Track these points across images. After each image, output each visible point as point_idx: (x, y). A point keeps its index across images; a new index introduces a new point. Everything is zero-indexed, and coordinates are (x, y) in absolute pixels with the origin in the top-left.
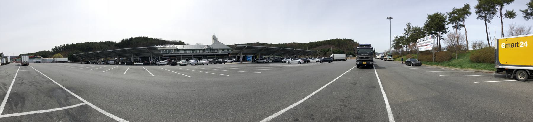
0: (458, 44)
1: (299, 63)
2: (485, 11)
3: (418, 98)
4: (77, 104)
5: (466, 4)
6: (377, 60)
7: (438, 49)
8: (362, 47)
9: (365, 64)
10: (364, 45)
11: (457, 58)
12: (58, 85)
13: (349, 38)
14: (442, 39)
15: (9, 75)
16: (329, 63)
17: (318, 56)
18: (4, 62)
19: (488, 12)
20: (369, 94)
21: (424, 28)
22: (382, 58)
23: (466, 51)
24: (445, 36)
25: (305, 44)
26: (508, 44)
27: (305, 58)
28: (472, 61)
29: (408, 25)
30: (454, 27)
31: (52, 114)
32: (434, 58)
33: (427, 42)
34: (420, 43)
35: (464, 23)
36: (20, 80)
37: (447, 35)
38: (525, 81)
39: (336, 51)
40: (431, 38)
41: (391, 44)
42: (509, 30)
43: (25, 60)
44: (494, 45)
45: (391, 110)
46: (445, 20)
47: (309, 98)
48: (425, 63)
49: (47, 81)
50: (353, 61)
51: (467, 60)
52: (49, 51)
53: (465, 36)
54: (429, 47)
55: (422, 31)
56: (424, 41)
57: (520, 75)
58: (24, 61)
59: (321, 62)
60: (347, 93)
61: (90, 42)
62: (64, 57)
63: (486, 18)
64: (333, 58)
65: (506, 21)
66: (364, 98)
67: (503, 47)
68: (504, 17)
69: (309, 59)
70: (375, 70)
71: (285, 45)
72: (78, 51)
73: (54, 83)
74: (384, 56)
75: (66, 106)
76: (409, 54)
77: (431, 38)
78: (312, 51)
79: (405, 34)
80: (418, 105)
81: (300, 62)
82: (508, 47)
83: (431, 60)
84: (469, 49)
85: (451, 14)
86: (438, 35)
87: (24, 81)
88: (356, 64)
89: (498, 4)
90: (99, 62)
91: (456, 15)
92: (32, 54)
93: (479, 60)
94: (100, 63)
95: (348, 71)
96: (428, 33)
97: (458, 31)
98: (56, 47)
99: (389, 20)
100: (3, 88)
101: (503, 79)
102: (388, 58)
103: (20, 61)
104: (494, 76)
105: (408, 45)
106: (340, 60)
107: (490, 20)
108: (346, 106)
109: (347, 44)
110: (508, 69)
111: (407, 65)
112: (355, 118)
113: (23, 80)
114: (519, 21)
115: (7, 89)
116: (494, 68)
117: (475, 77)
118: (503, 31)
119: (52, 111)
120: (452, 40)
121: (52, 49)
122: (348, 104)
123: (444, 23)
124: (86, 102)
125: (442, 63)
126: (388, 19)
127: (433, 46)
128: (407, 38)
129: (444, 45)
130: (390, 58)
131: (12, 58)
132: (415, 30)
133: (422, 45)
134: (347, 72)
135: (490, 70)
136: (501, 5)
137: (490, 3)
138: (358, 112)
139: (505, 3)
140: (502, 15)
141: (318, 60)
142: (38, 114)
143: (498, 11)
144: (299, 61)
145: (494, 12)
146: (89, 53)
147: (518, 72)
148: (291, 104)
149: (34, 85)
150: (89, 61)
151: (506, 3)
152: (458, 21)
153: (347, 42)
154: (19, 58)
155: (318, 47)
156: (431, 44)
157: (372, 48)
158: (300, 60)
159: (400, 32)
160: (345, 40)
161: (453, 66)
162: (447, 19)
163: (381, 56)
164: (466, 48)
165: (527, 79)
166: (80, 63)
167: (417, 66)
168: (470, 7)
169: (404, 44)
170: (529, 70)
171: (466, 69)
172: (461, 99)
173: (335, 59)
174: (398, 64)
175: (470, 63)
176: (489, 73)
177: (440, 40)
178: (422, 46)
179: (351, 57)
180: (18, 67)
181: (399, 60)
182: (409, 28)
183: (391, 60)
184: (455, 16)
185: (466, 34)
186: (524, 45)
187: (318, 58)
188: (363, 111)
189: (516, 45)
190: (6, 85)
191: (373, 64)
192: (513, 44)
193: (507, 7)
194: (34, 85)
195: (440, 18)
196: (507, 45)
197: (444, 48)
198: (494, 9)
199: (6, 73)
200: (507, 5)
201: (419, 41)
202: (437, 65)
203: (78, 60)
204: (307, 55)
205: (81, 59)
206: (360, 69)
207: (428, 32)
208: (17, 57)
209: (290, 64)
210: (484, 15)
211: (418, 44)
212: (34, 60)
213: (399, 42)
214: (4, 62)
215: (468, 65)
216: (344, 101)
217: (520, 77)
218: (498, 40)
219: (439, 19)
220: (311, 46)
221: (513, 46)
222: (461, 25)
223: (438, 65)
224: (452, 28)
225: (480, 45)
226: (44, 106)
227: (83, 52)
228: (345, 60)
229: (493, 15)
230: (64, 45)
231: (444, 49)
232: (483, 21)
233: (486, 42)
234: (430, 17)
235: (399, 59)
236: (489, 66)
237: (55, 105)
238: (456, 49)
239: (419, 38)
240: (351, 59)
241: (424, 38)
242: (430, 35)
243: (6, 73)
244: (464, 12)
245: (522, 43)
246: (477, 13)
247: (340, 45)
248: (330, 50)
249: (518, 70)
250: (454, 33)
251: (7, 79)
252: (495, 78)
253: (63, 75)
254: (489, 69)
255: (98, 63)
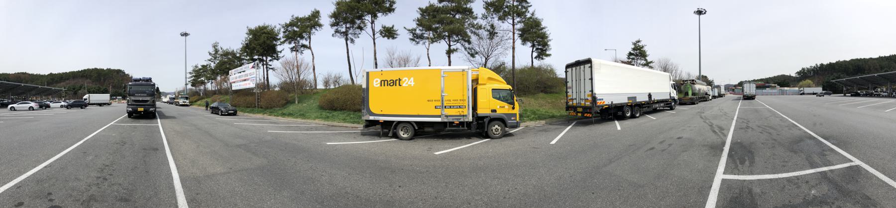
0: (299, 79)
1: (31, 108)
2: (345, 23)
3: (231, 169)
4: (841, 164)
5: (315, 9)
6: (161, 105)
7: (265, 86)
8: (137, 82)
9: (141, 112)
10: (140, 80)
11: (297, 102)
12: (808, 133)
13: (116, 68)
14: (272, 69)
15: (725, 114)
16: (82, 108)
17: (63, 97)
18: (716, 94)
19: (351, 25)
20: (145, 161)
21: (240, 51)
22: (172, 101)
23: (312, 90)
24: (275, 64)
25: (42, 76)
26: (384, 81)
27: (41, 100)
28: (322, 108)
29: (215, 46)
30: (292, 49)
31: (798, 179)
32: (258, 102)
33: (246, 75)
34: (234, 76)
35: (310, 42)
36: (743, 122)
37: (281, 63)
38: (411, 139)
39: (93, 89)
40: (253, 67)
41: (186, 78)
42: (386, 57)
43: (750, 90)
44: (360, 81)
45: (183, 188)
46: (278, 36)
47: (45, 167)
48: (243, 110)
49: (787, 126)
50: (121, 106)
51: (314, 105)
52: (792, 75)
53: (311, 64)
54: (250, 84)
55: (238, 55)
56: (240, 72)
57: (403, 130)
58: (748, 92)
59: (69, 107)
60: (109, 157)
61: (861, 59)
62: (817, 85)
63: (347, 35)
64: (88, 100)
65: (382, 41)
66: (136, 167)
67: (377, 84)
68: (378, 35)
69: (48, 103)
70: (159, 120)
71: (6, 77)
72: (839, 74)
73: (800, 129)
74: (174, 99)
75: (821, 167)
76: (217, 95)
77: (253, 67)
78: (53, 88)
79: (209, 60)
80: (231, 180)
81: (32, 107)
82: (384, 86)
83: (253, 105)
84: (318, 88)
85: (288, 27)
86: (265, 63)
87: (750, 125)
88: (127, 110)
89: (369, 13)
90: (877, 93)
91: (295, 29)
92: (761, 80)
93: (334, 106)
94: (879, 95)
95: (112, 123)
96: (248, 60)
97: (299, 55)
98: (803, 69)
99: (184, 37)
100: (719, 134)
101: (376, 137)
102: (181, 101)
103: (741, 91)
104: (360, 134)
105: (215, 79)
106: (100, 105)
107: (354, 38)
108: (106, 180)
109: (113, 78)
110: (384, 121)
111: (212, 113)
112: (119, 200)
113: (749, 123)
114: (403, 44)
115: (726, 136)
116: (360, 121)
117: (328, 134)
118: (376, 59)
119: (798, 175)
120: (289, 71)
121: (796, 73)
122: (109, 176)
123: (275, 42)
124: (857, 162)
125: (271, 110)
126: (182, 35)
127: (256, 80)
128: (213, 67)
129: (275, 80)
130: (185, 101)
131: (728, 88)
132: (226, 54)
133: (238, 79)
134: (110, 124)
135: (354, 122)
136: (374, 16)
137: (356, 11)
138: (125, 189)
139: (379, 12)
140: (375, 33)
141: (63, 103)
142: (776, 179)
143: (369, 25)
144: (30, 105)
145: (362, 25)
146: (858, 77)
147: (401, 126)
148: (11, 180)
149: (767, 132)
150: (859, 92)
151: (382, 12)
152: (298, 39)
153: (112, 74)
154: (739, 88)
155: (63, 82)
156: (253, 79)
157: (154, 85)
158: (33, 104)
159: (202, 58)
160: (109, 70)
161: (290, 115)
162: (281, 35)
163: (170, 98)
164: (313, 84)
165: (414, 136)
166: (843, 95)
167: (229, 115)
168: (321, 16)
169: (209, 79)
170: (416, 122)
171: (313, 121)
172: (305, 171)
173: (91, 102)
174: (199, 113)
175: (320, 111)
176: (352, 127)
177: (267, 71)
178: (237, 82)
179: (119, 99)
180: (738, 101)
181: (199, 105)
182: (216, 51)
183: (187, 105)
184: (294, 30)
185: (313, 61)
186: (409, 83)
187: (63, 101)
188: (134, 188)
189: (398, 82)
190: (723, 130)
191: (155, 110)
192: (392, 81)
193: (383, 20)
194: (767, 132)
195: (268, 33)
196: (383, 83)
197: (275, 86)
198: (361, 22)
199: (721, 111)
200: (383, 16)
201: (233, 73)
202: (264, 114)
203: (840, 89)
204: (44, 96)
205: (844, 89)
206: (133, 120)
207: (248, 58)
208: (735, 86)
209: (15, 110)
210: (344, 30)
211: (231, 78)
212: (764, 91)
213: (200, 75)
214: (716, 94)
215: (315, 115)
216: (102, 170)
217: (404, 134)
218: (368, 73)
219: (267, 35)
220: (53, 79)
221: (392, 84)
222: (304, 46)
223: (265, 113)
224: (289, 51)
225: (336, 81)
226: (784, 166)
227: (847, 75)
228: (109, 104)
229: (359, 30)
230: (816, 65)
231: (275, 86)
232: (343, 40)
233: (346, 77)
234: (251, 32)
235: (199, 102)
236: (352, 116)
237: (804, 165)
238: (295, 87)
239: (231, 67)
240: (119, 103)
241: (240, 68)
242: (251, 63)
243: (721, 111)
244: (310, 23)
245: (405, 80)
246: (332, 25)
247: (100, 80)
248: (84, 86)
249: (399, 122)
250: (292, 59)
251: (723, 120)
252: (362, 136)
253: (815, 116)
254: (352, 121)
255: (874, 95)
